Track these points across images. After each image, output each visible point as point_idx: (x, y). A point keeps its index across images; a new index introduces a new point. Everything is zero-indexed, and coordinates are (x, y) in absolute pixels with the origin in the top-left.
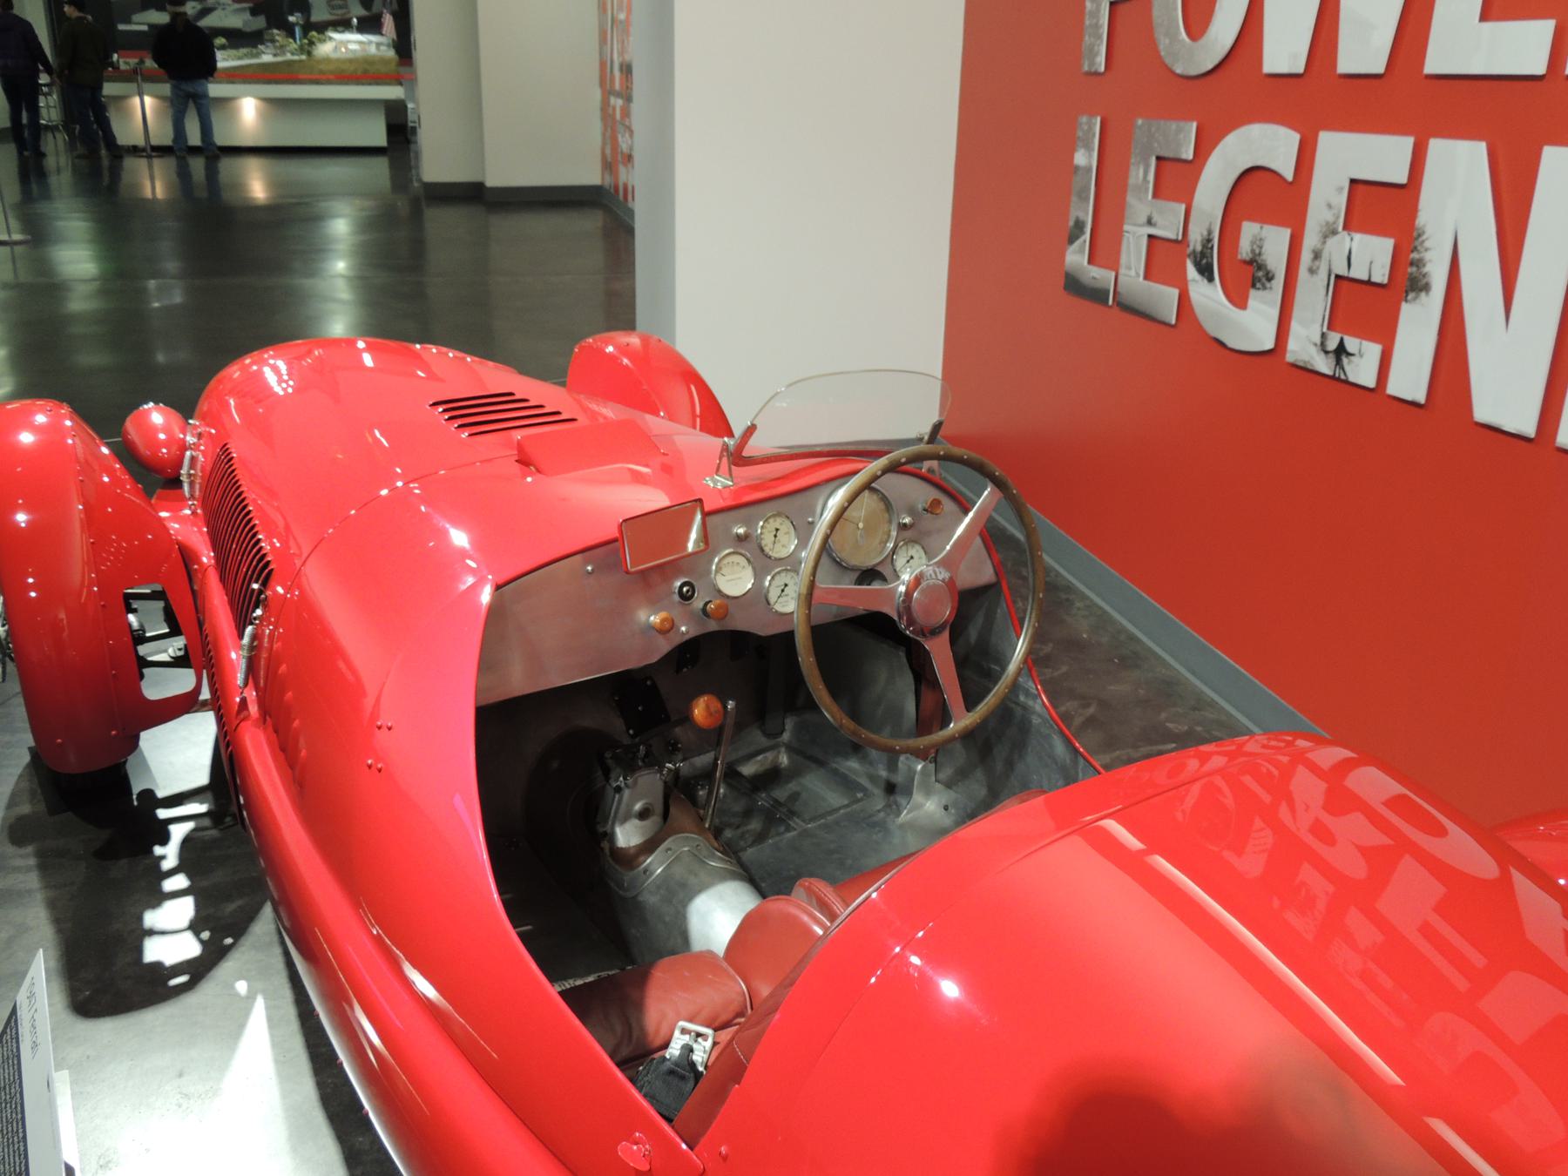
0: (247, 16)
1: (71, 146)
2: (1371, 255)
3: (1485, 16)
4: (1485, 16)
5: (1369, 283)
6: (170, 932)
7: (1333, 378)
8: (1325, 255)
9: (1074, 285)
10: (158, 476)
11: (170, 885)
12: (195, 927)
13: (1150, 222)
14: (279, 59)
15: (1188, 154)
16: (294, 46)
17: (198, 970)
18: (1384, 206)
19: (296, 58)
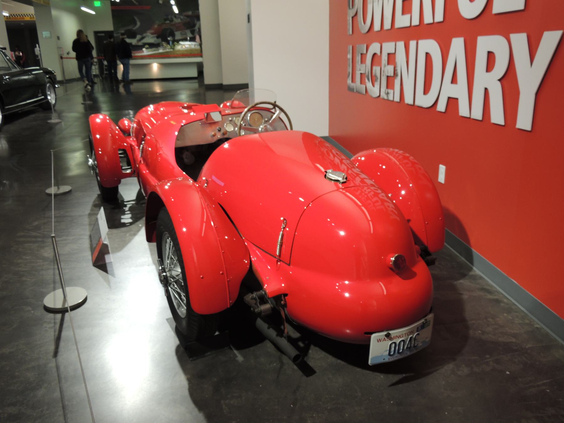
0: (156, 39)
1: (67, 169)
2: (389, 70)
6: (127, 218)
9: (351, 90)
10: (126, 132)
11: (126, 213)
12: (131, 218)
14: (165, 51)
15: (365, 52)
16: (169, 47)
17: (131, 224)
18: (391, 58)
19: (170, 50)
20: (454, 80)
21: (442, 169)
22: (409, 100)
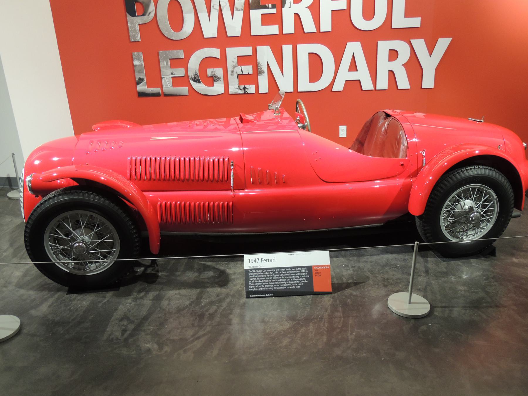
2: (248, 69)
3: (357, 70)
4: (357, 70)
5: (249, 74)
7: (244, 94)
8: (235, 71)
13: (172, 74)
18: (252, 60)
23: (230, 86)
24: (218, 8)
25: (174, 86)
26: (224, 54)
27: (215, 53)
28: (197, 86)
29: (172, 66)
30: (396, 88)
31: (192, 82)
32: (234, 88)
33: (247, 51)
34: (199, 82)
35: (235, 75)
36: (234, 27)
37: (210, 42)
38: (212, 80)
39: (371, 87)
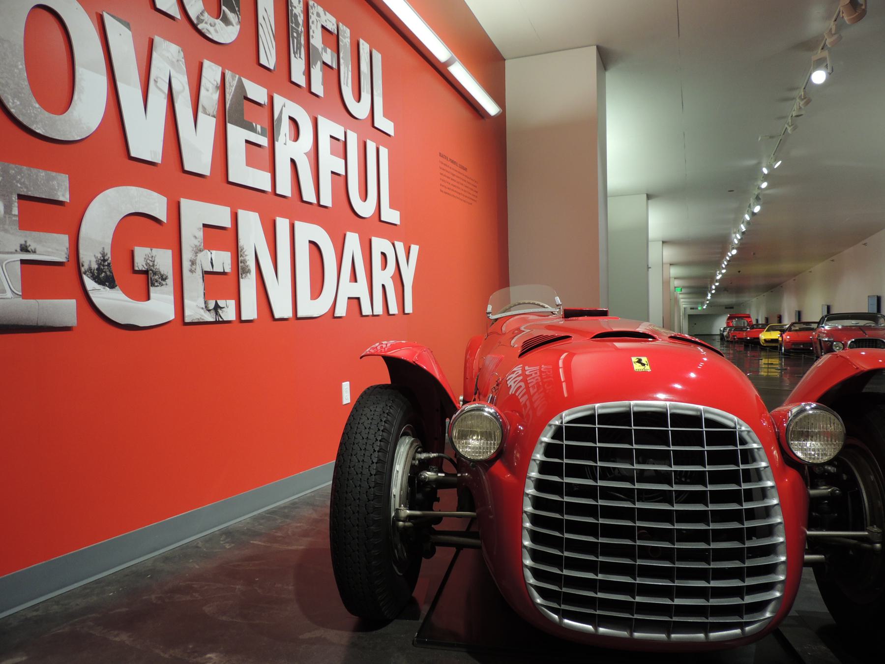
2: (222, 260)
8: (198, 262)
13: (24, 249)
18: (223, 237)
20: (354, 278)
21: (346, 386)
22: (282, 309)
23: (186, 301)
24: (166, 89)
25: (25, 295)
26: (175, 211)
27: (156, 205)
28: (109, 300)
29: (26, 223)
30: (269, 319)
31: (90, 284)
32: (195, 310)
33: (220, 215)
34: (112, 286)
35: (199, 274)
36: (198, 156)
37: (140, 172)
38: (145, 281)
39: (289, 314)
